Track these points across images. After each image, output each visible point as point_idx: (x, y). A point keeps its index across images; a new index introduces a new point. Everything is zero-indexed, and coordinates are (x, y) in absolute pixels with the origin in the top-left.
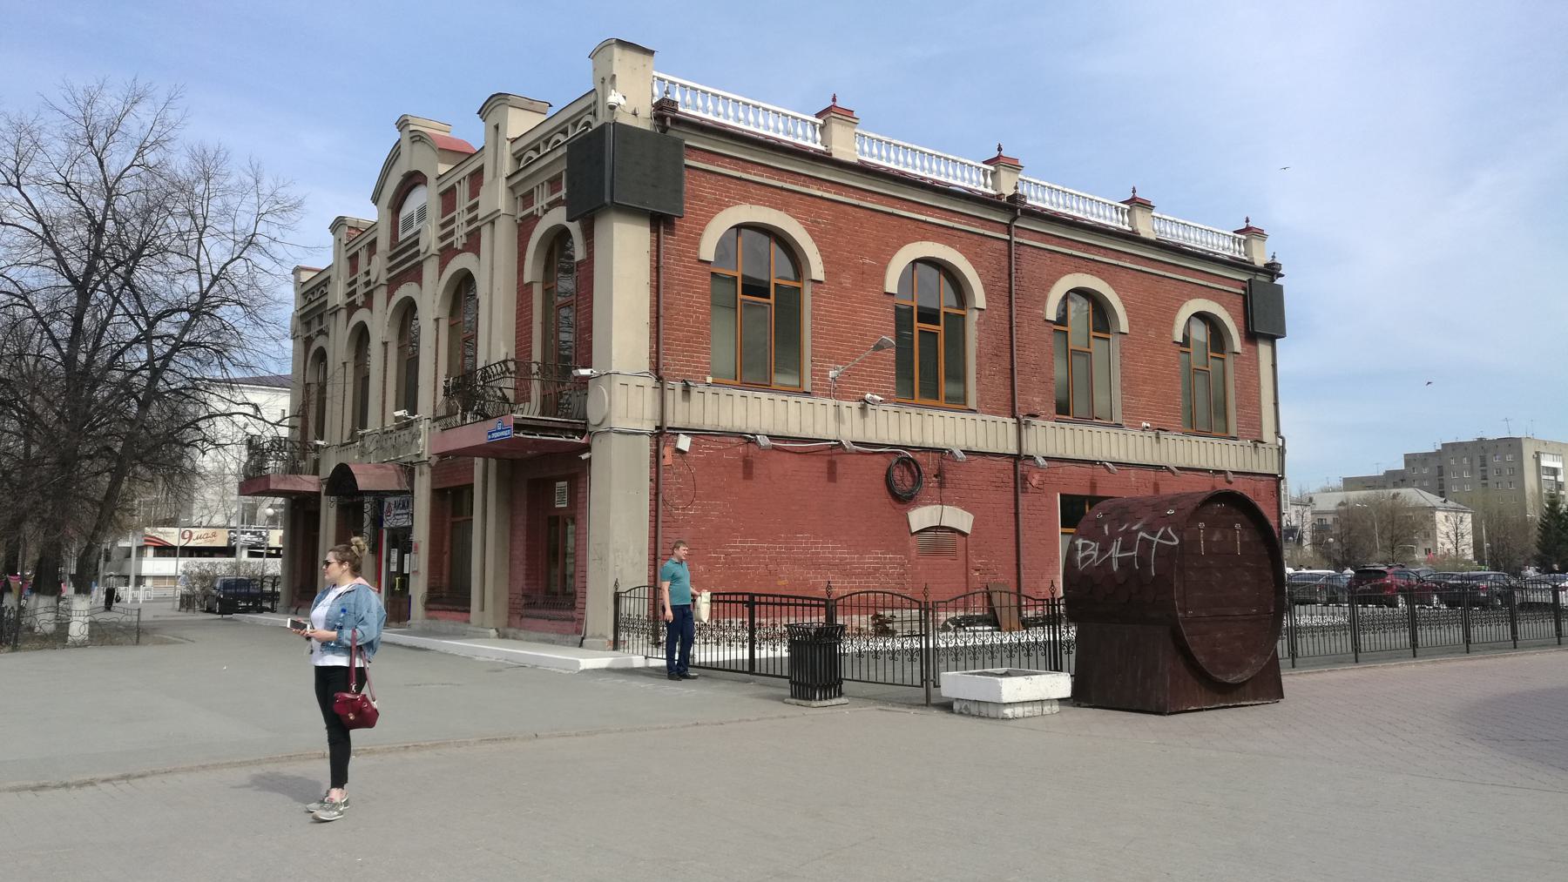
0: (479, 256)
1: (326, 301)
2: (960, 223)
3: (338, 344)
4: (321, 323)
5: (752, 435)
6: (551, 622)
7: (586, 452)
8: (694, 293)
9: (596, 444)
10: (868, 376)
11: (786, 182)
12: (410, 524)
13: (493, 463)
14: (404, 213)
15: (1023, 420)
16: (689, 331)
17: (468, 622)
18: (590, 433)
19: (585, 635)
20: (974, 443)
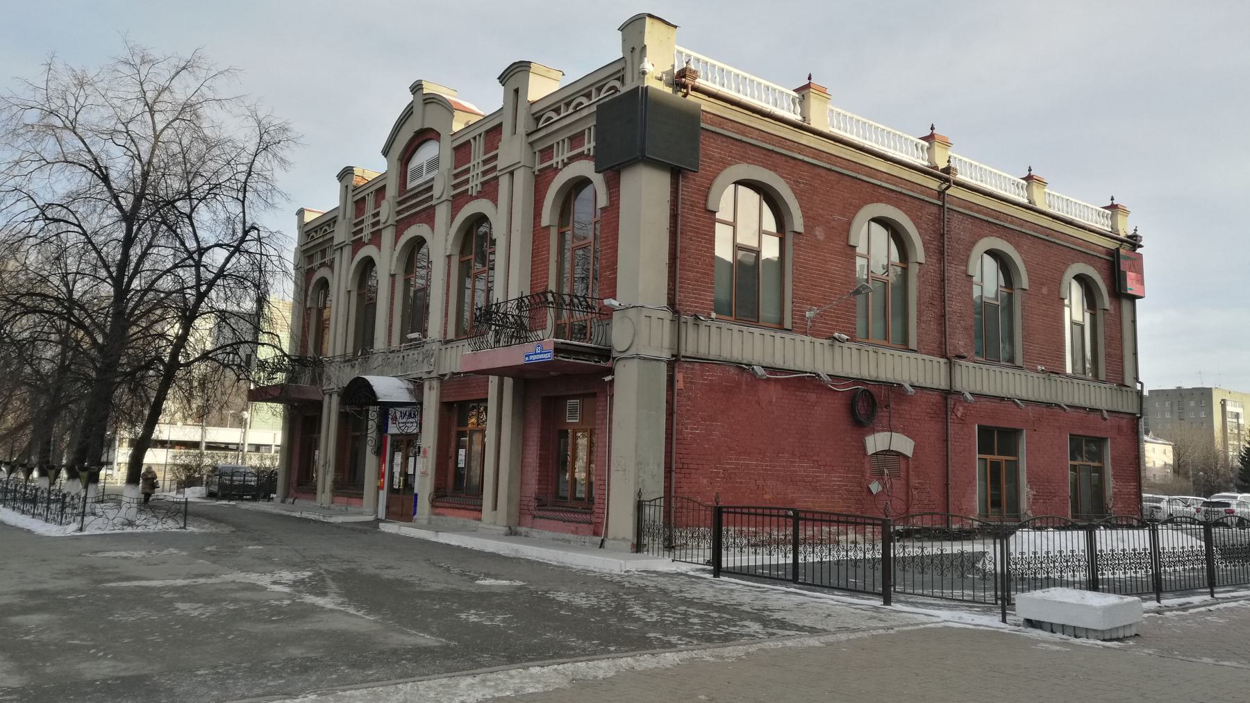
1: (333, 237)
3: (342, 278)
4: (323, 256)
5: (746, 365)
6: (567, 523)
7: (608, 375)
9: (620, 369)
10: (835, 317)
12: (413, 429)
13: (508, 382)
14: (413, 164)
15: (951, 358)
17: (480, 520)
18: (614, 358)
20: (916, 379)
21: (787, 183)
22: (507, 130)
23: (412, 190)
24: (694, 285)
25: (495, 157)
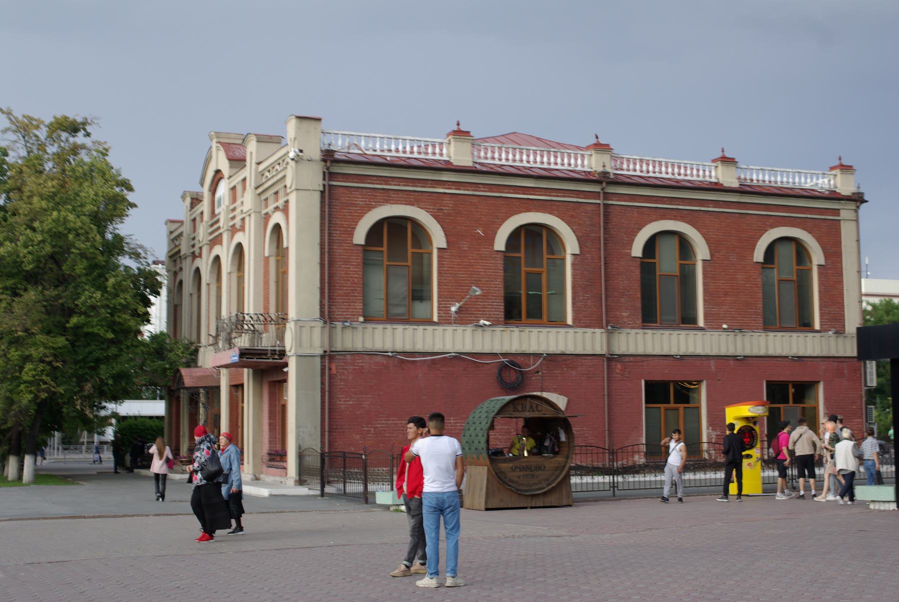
2: (558, 196)
5: (392, 352)
16: (347, 290)
21: (428, 212)
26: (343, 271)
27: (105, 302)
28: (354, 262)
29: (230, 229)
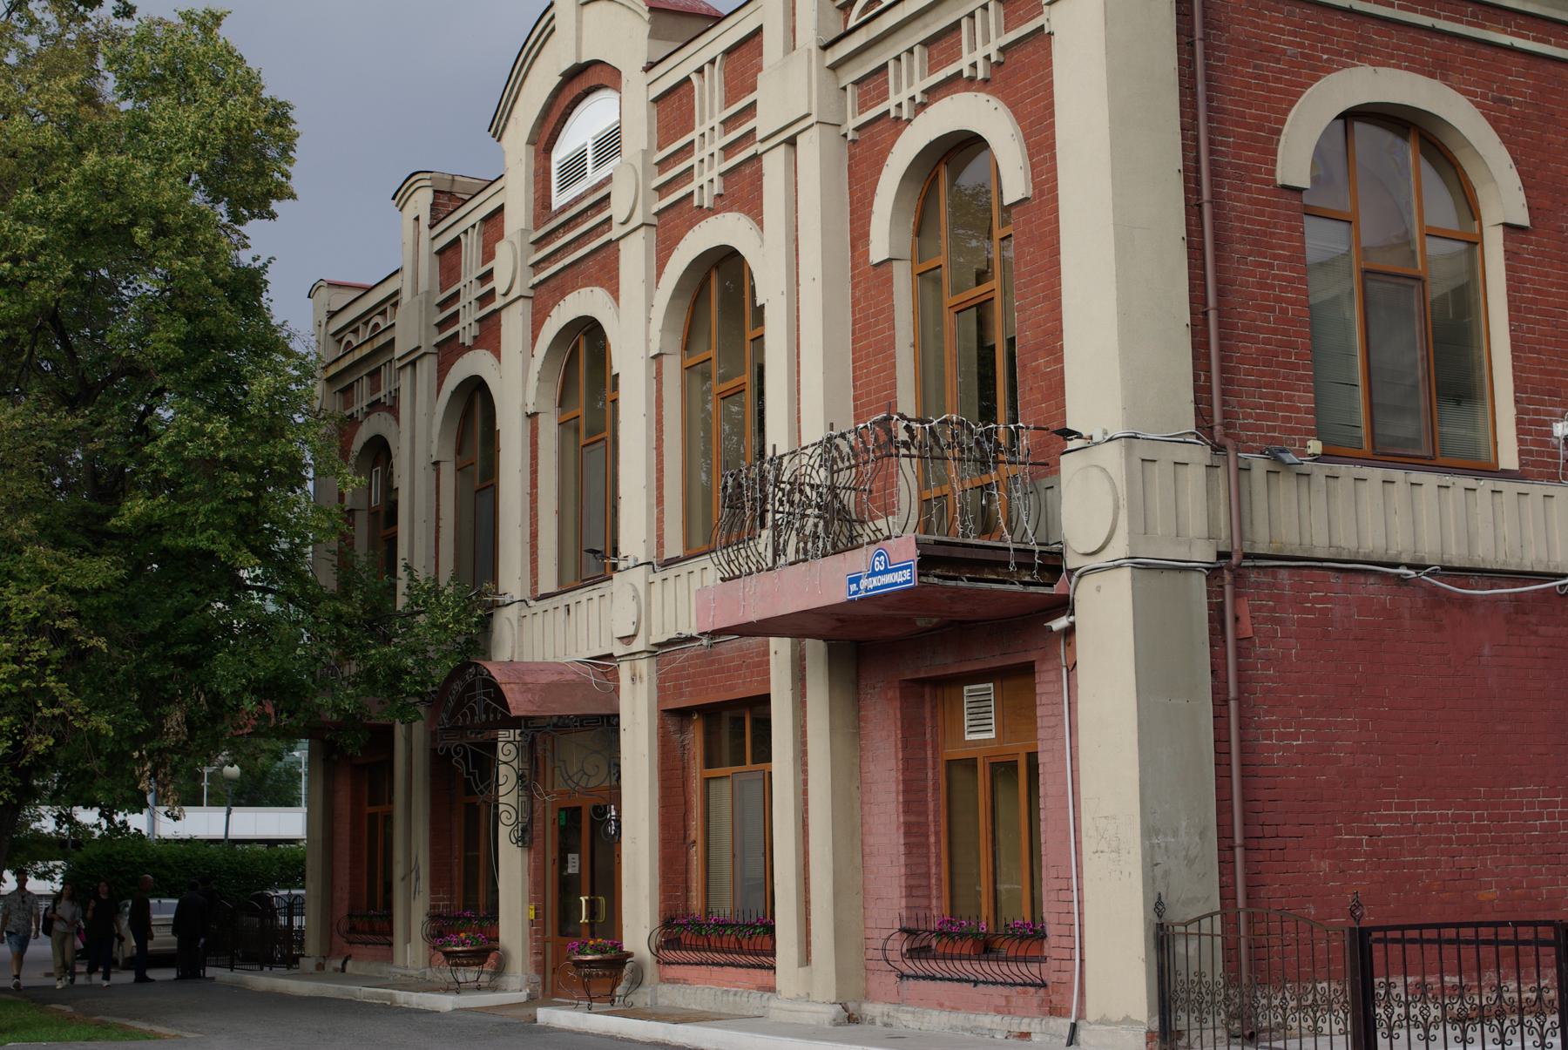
0: (760, 223)
1: (392, 341)
4: (375, 388)
8: (1276, 257)
11: (1438, 17)
13: (815, 650)
14: (562, 152)
17: (772, 989)
19: (1081, 1014)
22: (772, 43)
23: (563, 209)
24: (1262, 373)
25: (751, 109)
26: (1252, 274)
27: (238, 451)
28: (1282, 247)
29: (655, 221)
